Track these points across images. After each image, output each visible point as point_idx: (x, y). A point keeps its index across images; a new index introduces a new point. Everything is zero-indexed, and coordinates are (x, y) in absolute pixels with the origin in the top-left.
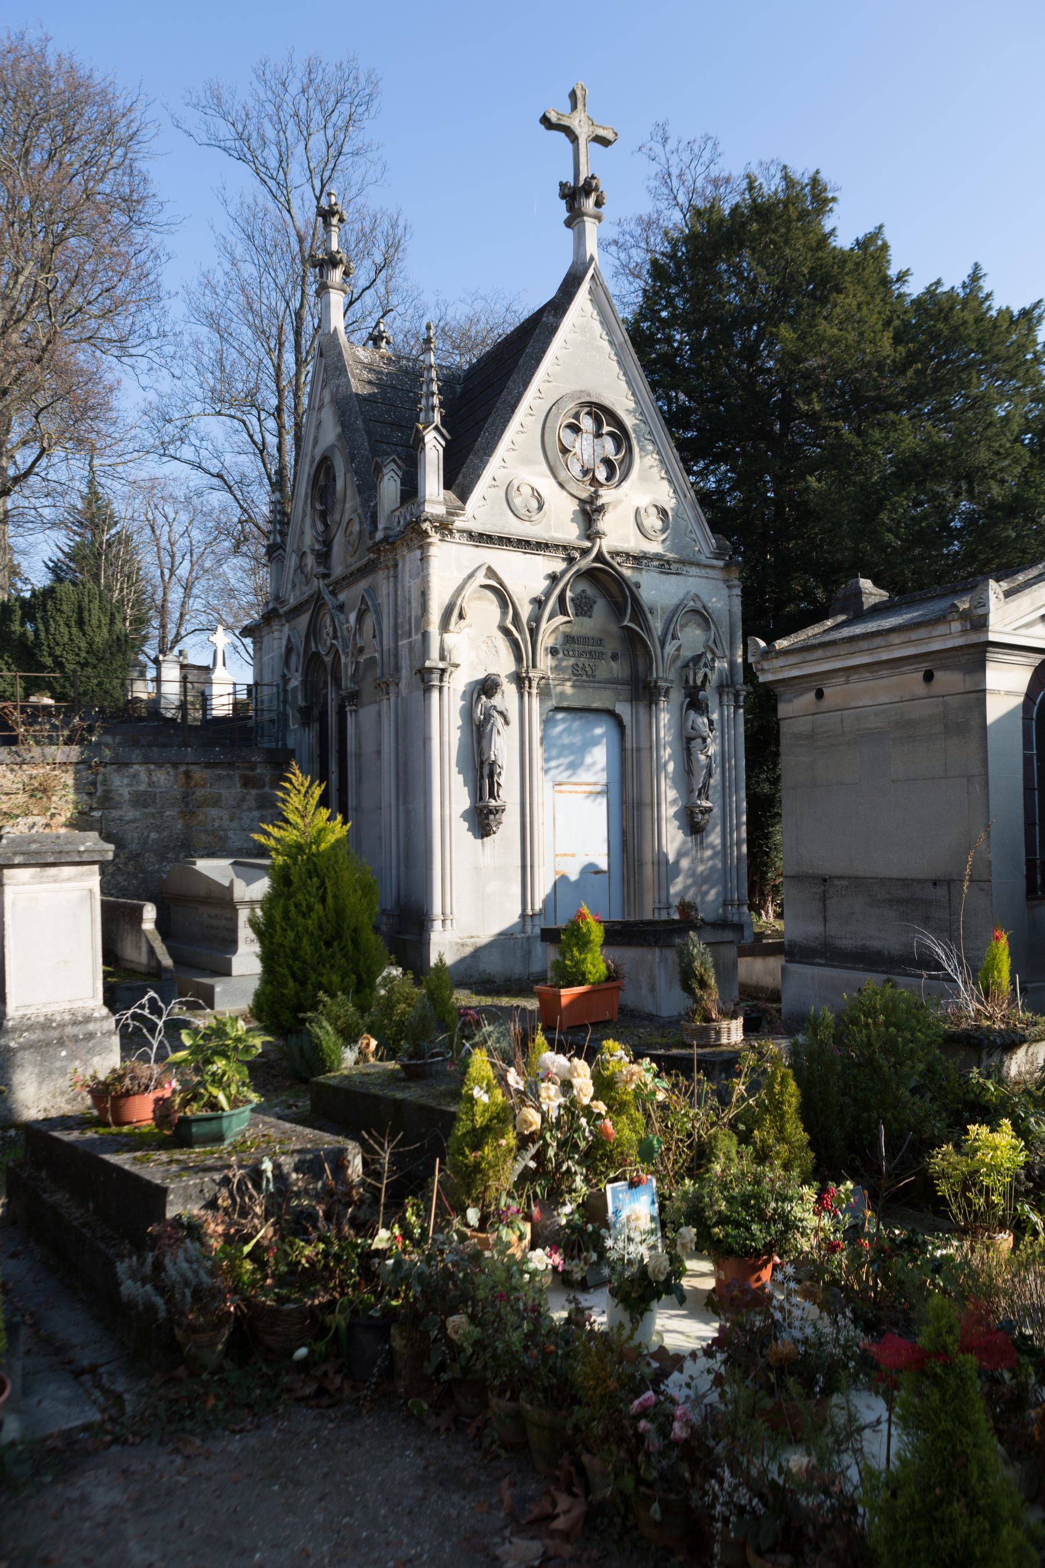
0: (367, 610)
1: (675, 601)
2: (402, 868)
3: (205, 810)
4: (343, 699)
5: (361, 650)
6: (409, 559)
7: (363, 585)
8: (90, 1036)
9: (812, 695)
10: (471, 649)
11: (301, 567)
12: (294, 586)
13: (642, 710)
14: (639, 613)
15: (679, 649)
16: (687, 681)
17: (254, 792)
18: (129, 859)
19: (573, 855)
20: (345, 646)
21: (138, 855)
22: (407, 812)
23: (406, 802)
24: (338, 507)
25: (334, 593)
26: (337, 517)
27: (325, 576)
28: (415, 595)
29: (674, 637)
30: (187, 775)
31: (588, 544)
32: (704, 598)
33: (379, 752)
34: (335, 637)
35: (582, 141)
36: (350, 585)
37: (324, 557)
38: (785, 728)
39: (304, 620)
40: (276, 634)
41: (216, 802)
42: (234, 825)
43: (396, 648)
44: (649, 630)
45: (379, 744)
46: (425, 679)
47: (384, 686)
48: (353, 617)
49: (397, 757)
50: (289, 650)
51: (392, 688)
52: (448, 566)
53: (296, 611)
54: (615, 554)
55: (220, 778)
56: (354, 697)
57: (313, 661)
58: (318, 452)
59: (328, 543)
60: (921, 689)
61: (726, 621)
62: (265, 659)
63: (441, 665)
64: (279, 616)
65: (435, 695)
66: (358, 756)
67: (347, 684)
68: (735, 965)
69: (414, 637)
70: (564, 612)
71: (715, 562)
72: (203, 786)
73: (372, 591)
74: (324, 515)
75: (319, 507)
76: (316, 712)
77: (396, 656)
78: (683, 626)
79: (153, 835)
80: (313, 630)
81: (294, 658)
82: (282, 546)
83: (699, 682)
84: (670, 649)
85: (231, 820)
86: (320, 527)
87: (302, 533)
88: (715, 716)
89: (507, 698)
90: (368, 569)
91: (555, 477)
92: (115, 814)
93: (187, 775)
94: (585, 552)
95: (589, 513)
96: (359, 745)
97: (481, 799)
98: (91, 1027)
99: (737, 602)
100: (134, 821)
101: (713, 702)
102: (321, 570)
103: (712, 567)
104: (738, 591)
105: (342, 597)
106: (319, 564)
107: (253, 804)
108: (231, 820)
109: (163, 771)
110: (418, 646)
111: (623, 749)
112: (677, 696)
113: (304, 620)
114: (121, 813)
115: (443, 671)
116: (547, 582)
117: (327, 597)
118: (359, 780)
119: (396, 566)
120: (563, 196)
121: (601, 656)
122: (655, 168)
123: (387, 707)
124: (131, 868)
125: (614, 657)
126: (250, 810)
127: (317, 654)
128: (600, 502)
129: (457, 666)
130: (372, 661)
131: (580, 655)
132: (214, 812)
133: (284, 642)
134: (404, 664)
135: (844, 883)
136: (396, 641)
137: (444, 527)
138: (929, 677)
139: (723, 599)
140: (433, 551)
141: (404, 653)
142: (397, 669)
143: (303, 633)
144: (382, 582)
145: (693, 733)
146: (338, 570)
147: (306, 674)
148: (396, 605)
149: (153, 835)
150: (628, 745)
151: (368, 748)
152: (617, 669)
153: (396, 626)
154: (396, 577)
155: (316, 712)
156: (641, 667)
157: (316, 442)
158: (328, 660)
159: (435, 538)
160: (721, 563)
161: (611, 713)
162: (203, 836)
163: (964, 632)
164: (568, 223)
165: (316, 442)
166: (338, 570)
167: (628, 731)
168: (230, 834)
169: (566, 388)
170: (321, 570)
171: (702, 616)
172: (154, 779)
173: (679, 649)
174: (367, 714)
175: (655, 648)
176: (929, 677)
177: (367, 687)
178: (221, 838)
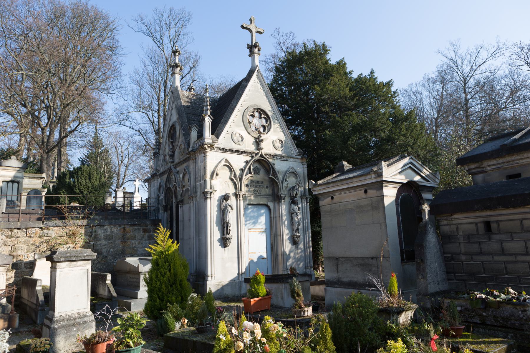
0: (186, 173)
1: (286, 169)
2: (197, 259)
3: (130, 241)
4: (178, 202)
5: (184, 186)
6: (200, 157)
7: (185, 165)
8: (85, 322)
9: (330, 198)
10: (220, 185)
11: (164, 160)
12: (162, 166)
13: (276, 204)
14: (275, 173)
15: (288, 184)
16: (291, 195)
17: (147, 234)
18: (103, 258)
19: (255, 253)
20: (179, 185)
21: (106, 257)
22: (199, 240)
23: (199, 237)
24: (177, 141)
25: (175, 168)
26: (177, 143)
27: (173, 162)
28: (202, 168)
29: (286, 181)
30: (124, 229)
32: (295, 168)
33: (190, 220)
34: (175, 182)
35: (254, 32)
36: (180, 165)
37: (172, 156)
38: (322, 209)
39: (165, 176)
40: (156, 181)
41: (134, 238)
42: (140, 245)
43: (196, 185)
44: (278, 178)
45: (190, 217)
46: (205, 195)
47: (191, 198)
48: (181, 175)
49: (260, 81)
50: (160, 186)
51: (194, 199)
52: (212, 159)
53: (163, 174)
54: (266, 155)
55: (135, 230)
56: (182, 201)
57: (168, 190)
58: (171, 124)
59: (173, 152)
60: (364, 196)
61: (302, 175)
62: (152, 189)
63: (210, 191)
64: (157, 176)
65: (208, 200)
66: (183, 221)
67: (179, 197)
68: (309, 289)
69: (201, 182)
70: (251, 173)
71: (298, 157)
72: (130, 233)
73: (188, 167)
74: (172, 143)
75: (171, 140)
76: (169, 207)
77: (196, 188)
78: (289, 177)
79: (112, 250)
80: (168, 180)
81: (161, 189)
82: (158, 153)
83: (294, 195)
84: (285, 184)
85: (139, 244)
86: (171, 147)
87: (165, 148)
88: (300, 206)
89: (232, 201)
90: (186, 160)
91: (247, 131)
92: (98, 243)
93: (124, 229)
96: (183, 217)
97: (224, 235)
98: (85, 319)
99: (306, 169)
100: (105, 245)
101: (299, 201)
102: (171, 160)
103: (297, 158)
104: (306, 166)
105: (178, 169)
106: (170, 158)
107: (147, 238)
108: (139, 244)
109: (116, 227)
110: (203, 185)
111: (271, 217)
112: (287, 199)
113: (165, 176)
114: (100, 242)
115: (211, 193)
116: (245, 164)
117: (173, 169)
118: (183, 229)
119: (196, 159)
120: (248, 48)
121: (263, 187)
122: (276, 40)
123: (193, 205)
124: (103, 262)
125: (267, 187)
126: (145, 240)
127: (169, 188)
128: (261, 139)
129: (216, 191)
130: (188, 190)
131: (256, 187)
132: (133, 241)
133: (158, 184)
134: (198, 190)
135: (344, 259)
136: (196, 183)
137: (211, 147)
138: (366, 192)
139: (301, 168)
140: (208, 154)
141: (198, 187)
142: (196, 192)
143: (165, 181)
144: (191, 164)
145: (293, 211)
146: (177, 160)
147: (166, 194)
148: (196, 176)
149: (112, 250)
150: (272, 216)
151: (186, 218)
152: (268, 191)
153: (196, 178)
154: (196, 162)
155: (169, 207)
156: (276, 191)
157: (170, 120)
158: (173, 189)
159: (208, 150)
160: (300, 157)
161: (266, 205)
162: (129, 250)
163: (376, 177)
164: (250, 56)
165: (170, 120)
166: (177, 160)
167: (272, 211)
168: (138, 249)
169: (250, 104)
170: (171, 160)
171: (295, 174)
172: (113, 230)
173: (288, 184)
174: (186, 207)
175: (280, 184)
176: (366, 192)
177: (186, 198)
178: (135, 250)
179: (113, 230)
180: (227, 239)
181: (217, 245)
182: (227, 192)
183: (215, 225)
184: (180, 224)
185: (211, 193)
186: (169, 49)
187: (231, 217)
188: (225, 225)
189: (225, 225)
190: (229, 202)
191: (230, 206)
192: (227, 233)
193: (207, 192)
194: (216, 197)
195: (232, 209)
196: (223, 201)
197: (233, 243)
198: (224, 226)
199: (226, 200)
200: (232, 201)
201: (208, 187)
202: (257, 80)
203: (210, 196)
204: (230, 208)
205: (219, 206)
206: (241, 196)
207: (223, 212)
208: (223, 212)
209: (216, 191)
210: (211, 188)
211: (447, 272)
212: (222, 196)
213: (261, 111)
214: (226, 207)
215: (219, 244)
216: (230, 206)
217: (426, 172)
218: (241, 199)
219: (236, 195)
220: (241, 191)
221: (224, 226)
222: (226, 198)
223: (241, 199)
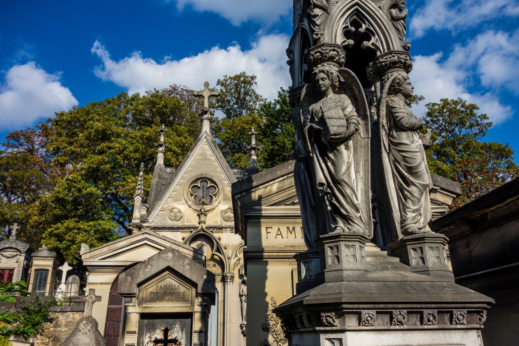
31: (198, 225)
94: (197, 228)
95: (201, 214)
172: (75, 316)
179: (75, 316)
184: (282, 260)
202: (207, 147)
213: (204, 179)
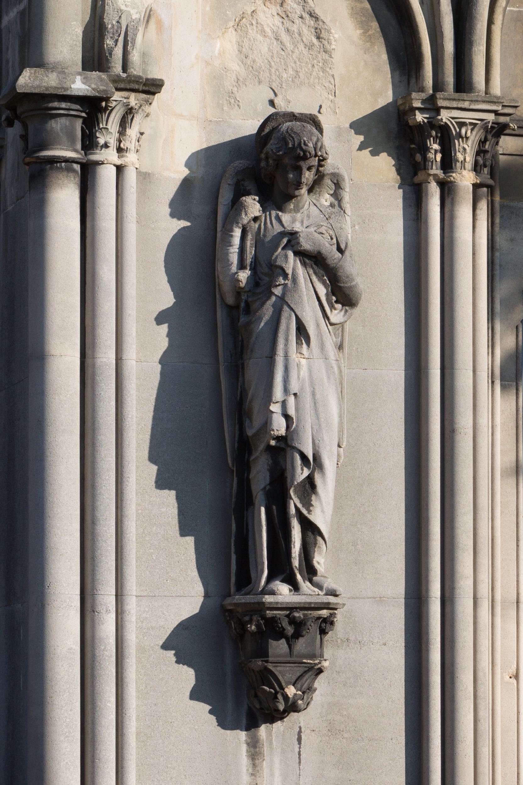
65: (64, 199)
89: (361, 207)
97: (245, 579)
115: (93, 108)
129: (152, 87)
180: (272, 628)
181: (162, 700)
182: (297, 102)
183: (141, 471)
185: (93, 108)
186: (325, 111)
187: (333, 391)
188: (260, 477)
189: (260, 477)
190: (306, 217)
191: (315, 260)
192: (281, 569)
193: (41, 105)
194: (166, 142)
195: (342, 294)
196: (236, 205)
197: (360, 671)
198: (240, 479)
199: (277, 195)
200: (361, 207)
201: (64, 39)
203: (89, 143)
204: (307, 292)
205: (195, 262)
206: (466, 151)
207: (228, 329)
208: (228, 329)
209: (152, 87)
210: (95, 57)
211: (4, 139)
212: (236, 147)
214: (266, 272)
215: (187, 676)
216: (315, 260)
217: (244, 276)
218: (465, 179)
219: (407, 138)
220: (463, 84)
221: (240, 479)
222: (270, 163)
223: (465, 179)
